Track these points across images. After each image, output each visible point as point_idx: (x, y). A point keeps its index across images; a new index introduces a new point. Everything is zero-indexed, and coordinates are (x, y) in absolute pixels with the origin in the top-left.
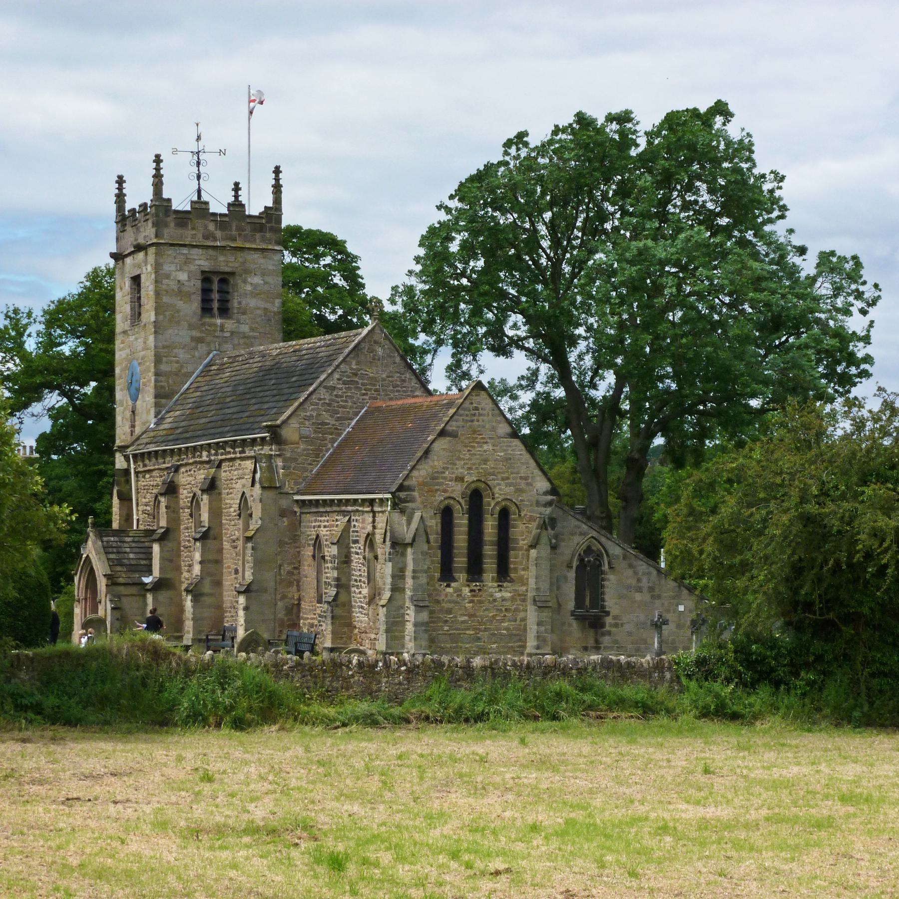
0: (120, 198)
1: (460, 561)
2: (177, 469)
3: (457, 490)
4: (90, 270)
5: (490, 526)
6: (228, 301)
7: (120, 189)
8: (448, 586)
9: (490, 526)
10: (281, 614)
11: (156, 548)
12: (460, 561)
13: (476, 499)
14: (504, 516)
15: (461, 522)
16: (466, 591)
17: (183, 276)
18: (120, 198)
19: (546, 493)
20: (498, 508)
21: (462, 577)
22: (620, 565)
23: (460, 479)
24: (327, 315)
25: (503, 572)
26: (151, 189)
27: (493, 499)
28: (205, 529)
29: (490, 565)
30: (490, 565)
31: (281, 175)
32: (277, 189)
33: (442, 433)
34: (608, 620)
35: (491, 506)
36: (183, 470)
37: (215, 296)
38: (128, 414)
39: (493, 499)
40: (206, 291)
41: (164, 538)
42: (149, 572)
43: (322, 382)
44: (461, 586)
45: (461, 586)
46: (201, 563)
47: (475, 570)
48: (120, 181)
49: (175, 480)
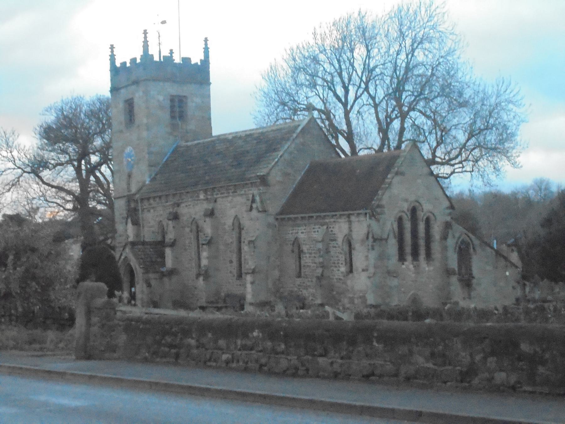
0: (113, 58)
1: (408, 249)
2: (178, 205)
3: (406, 206)
4: (267, 67)
5: (422, 227)
6: (183, 112)
7: (112, 52)
8: (403, 264)
9: (422, 227)
10: (270, 285)
11: (168, 252)
12: (408, 249)
13: (414, 211)
14: (428, 221)
15: (408, 225)
16: (411, 266)
17: (161, 98)
18: (113, 58)
19: (447, 208)
20: (425, 217)
21: (409, 258)
22: (479, 250)
23: (406, 200)
24: (61, 145)
25: (429, 255)
26: (141, 49)
27: (423, 212)
28: (208, 238)
29: (422, 256)
30: (422, 256)
31: (208, 42)
32: (206, 51)
33: (397, 173)
34: (474, 281)
35: (421, 215)
36: (183, 205)
37: (177, 109)
38: (125, 177)
39: (423, 212)
40: (172, 107)
41: (172, 245)
42: (163, 264)
43: (286, 150)
44: (409, 264)
45: (409, 264)
46: (208, 258)
47: (415, 254)
48: (112, 47)
49: (178, 211)
